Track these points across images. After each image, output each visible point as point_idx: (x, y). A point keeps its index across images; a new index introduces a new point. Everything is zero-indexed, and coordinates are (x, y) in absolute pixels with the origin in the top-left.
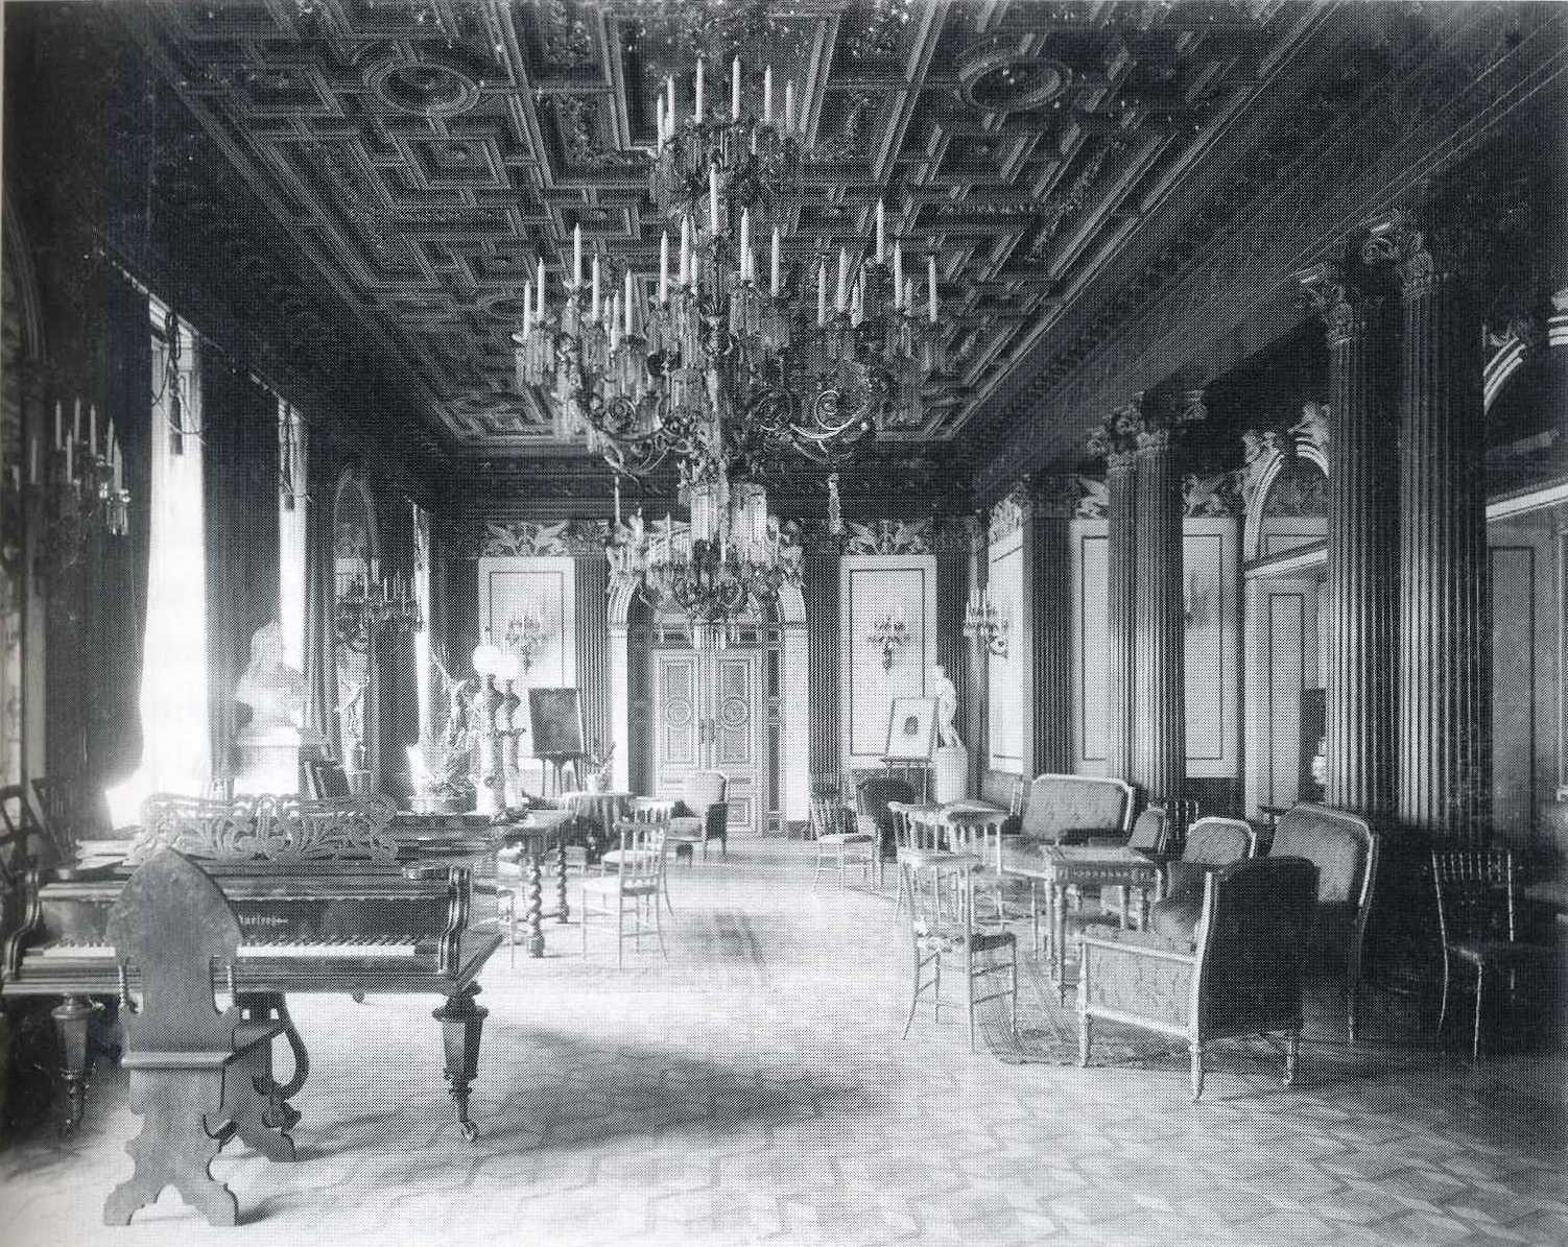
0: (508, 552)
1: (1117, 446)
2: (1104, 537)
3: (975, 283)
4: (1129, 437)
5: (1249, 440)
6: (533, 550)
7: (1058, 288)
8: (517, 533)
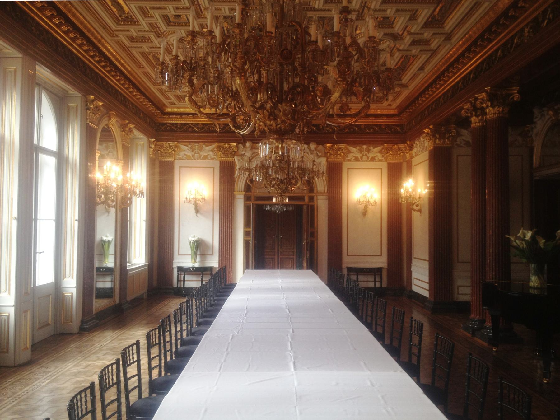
0: (357, 159)
1: (476, 113)
2: (469, 155)
3: (410, 33)
4: (483, 109)
5: (536, 111)
6: (368, 158)
7: (448, 37)
8: (361, 151)
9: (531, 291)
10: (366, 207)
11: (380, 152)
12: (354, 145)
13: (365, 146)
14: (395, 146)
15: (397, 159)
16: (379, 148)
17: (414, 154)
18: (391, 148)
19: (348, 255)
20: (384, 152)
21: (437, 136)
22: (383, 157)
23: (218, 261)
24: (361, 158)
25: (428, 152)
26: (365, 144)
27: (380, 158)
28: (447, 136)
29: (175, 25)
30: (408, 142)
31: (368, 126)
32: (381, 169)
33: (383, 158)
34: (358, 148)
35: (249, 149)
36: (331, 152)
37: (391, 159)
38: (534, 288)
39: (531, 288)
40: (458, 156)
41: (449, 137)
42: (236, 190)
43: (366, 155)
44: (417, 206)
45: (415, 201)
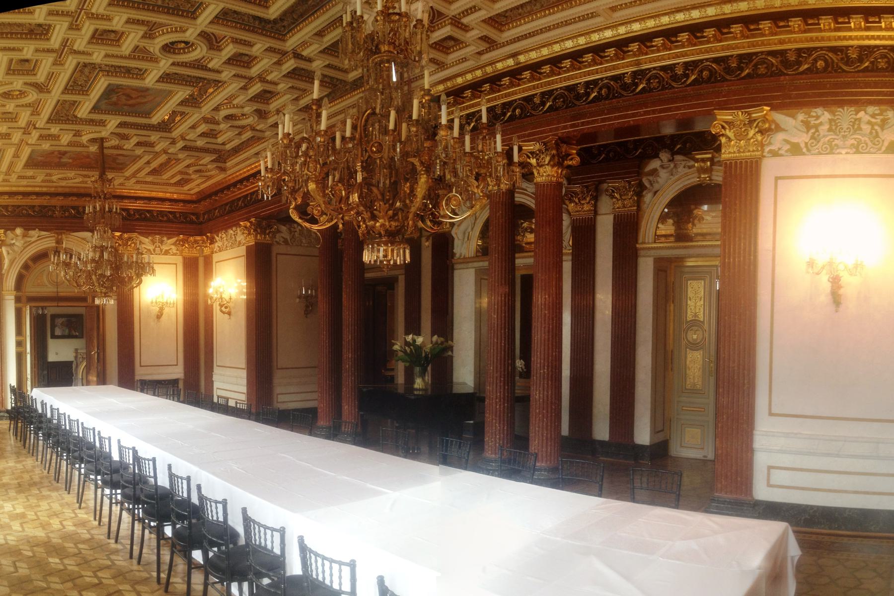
6: (161, 250)
8: (153, 242)
11: (174, 244)
14: (192, 239)
16: (174, 240)
17: (216, 249)
23: (473, 370)
24: (154, 250)
25: (244, 247)
26: (156, 234)
29: (14, 74)
31: (161, 213)
35: (20, 238)
37: (187, 252)
38: (419, 390)
39: (417, 390)
42: (4, 289)
44: (226, 308)
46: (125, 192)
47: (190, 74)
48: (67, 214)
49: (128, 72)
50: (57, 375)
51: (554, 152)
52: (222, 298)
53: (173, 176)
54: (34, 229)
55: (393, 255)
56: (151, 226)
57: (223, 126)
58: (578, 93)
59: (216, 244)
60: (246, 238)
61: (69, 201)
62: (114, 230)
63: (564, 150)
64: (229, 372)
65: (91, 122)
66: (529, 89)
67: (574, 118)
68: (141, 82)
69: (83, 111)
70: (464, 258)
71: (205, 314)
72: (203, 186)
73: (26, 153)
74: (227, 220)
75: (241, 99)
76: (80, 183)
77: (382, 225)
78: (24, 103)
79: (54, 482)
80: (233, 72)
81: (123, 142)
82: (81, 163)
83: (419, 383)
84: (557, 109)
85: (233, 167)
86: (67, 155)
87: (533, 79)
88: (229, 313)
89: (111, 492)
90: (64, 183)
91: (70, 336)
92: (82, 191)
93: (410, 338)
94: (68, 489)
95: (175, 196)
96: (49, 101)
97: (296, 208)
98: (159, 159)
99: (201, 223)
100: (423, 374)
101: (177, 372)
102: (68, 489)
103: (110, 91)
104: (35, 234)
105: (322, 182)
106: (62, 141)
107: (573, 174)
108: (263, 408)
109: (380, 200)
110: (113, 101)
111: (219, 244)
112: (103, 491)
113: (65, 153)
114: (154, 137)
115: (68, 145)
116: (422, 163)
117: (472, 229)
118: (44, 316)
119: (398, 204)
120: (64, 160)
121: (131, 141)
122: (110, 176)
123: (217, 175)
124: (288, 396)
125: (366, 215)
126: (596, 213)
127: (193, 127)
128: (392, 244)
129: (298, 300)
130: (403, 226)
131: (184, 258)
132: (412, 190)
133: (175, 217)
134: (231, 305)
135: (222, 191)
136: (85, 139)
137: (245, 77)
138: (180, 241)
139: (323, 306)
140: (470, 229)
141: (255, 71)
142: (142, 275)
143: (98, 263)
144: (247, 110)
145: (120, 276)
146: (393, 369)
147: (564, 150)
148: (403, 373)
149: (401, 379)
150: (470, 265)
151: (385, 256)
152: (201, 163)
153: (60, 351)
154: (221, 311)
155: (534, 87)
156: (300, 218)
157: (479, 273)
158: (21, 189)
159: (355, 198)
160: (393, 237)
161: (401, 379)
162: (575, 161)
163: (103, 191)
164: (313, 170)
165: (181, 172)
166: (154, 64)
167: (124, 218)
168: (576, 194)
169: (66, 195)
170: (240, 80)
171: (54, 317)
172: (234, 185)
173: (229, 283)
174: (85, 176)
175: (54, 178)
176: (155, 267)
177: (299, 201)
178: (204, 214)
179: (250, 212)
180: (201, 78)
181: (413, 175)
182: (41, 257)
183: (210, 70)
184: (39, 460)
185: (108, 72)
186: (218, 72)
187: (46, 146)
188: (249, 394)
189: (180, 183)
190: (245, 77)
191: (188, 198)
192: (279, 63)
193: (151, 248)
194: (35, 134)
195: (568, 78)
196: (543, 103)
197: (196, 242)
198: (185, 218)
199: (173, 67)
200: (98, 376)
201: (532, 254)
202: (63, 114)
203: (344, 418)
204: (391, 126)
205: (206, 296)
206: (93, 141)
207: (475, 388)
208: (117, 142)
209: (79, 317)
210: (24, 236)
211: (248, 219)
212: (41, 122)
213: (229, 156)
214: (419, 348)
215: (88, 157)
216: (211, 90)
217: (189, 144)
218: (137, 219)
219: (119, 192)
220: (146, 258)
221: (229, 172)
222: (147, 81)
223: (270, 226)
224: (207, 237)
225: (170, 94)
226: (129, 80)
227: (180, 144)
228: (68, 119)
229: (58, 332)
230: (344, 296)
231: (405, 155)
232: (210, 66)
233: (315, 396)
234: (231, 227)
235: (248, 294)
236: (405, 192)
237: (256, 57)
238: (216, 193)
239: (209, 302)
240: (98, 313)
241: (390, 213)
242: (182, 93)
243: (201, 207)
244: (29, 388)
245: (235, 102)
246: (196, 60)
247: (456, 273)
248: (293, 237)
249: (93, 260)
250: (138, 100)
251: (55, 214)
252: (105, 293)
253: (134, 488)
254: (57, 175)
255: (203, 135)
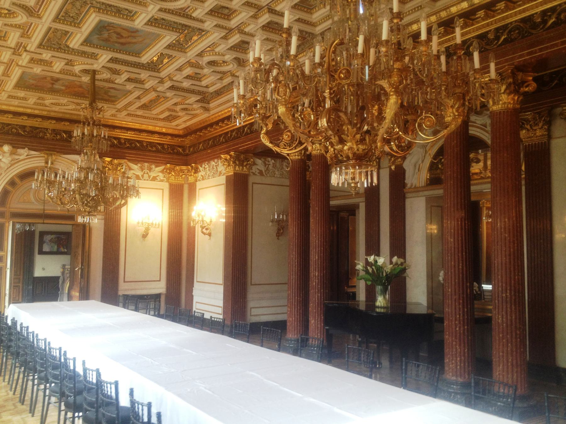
0: (138, 177)
6: (149, 177)
9: (378, 310)
10: (147, 229)
11: (162, 172)
12: (135, 162)
13: (146, 164)
14: (178, 168)
15: (180, 180)
18: (174, 169)
19: (124, 282)
20: (166, 172)
21: (237, 163)
22: (164, 177)
24: (143, 176)
25: (224, 177)
26: (146, 162)
27: (162, 178)
28: (245, 164)
30: (193, 165)
31: (151, 144)
32: (163, 189)
33: (165, 179)
34: (139, 165)
35: (8, 155)
36: (110, 167)
37: (173, 180)
38: (381, 307)
39: (378, 307)
40: (253, 183)
41: (247, 164)
43: (147, 173)
44: (207, 229)
45: (206, 225)
46: (117, 123)
47: (176, 21)
48: (58, 137)
49: (118, 11)
50: (43, 290)
51: (511, 80)
52: (203, 221)
53: (162, 112)
54: (24, 148)
55: (360, 178)
56: (140, 155)
57: (206, 71)
58: (535, 23)
59: (200, 174)
60: (226, 169)
61: (65, 126)
62: (102, 155)
63: (519, 78)
64: (207, 287)
65: (83, 54)
66: (483, 27)
67: (532, 46)
68: (131, 22)
69: (75, 42)
70: (415, 187)
71: (188, 235)
72: (188, 124)
73: (16, 74)
74: (209, 153)
75: (221, 48)
76: (74, 110)
77: (350, 148)
78: (10, 23)
79: (19, 405)
80: (215, 23)
81: (115, 76)
82: (74, 91)
83: (380, 301)
84: (512, 41)
85: (216, 107)
86: (60, 82)
87: (487, 17)
88: (210, 235)
89: (74, 415)
90: (56, 108)
91: (58, 253)
92: (75, 118)
93: (371, 259)
94: (32, 411)
95: (164, 130)
96: (40, 26)
97: (267, 133)
98: (149, 96)
99: (187, 155)
100: (384, 292)
101: (160, 287)
102: (32, 411)
103: (101, 28)
104: (24, 152)
105: (293, 108)
106: (54, 68)
107: (528, 101)
108: (238, 323)
109: (348, 124)
110: (104, 36)
111: (201, 173)
112: (66, 414)
113: (57, 80)
114: (144, 75)
115: (60, 72)
116: (391, 85)
117: (423, 161)
118: (31, 234)
119: (366, 128)
120: (57, 86)
121: (123, 76)
122: (100, 105)
123: (202, 114)
124: (261, 310)
125: (334, 140)
126: (550, 137)
127: (180, 69)
128: (360, 167)
129: (271, 224)
130: (370, 150)
131: (171, 185)
132: (380, 112)
133: (163, 148)
134: (211, 227)
135: (205, 128)
136: (77, 69)
137: (225, 28)
138: (167, 169)
139: (292, 230)
140: (420, 162)
141: (234, 23)
142: (127, 196)
143: (82, 183)
144: (228, 57)
145: (106, 198)
146: (355, 287)
147: (519, 78)
148: (364, 291)
149: (362, 296)
150: (421, 193)
151: (353, 179)
152: (187, 102)
153: (46, 266)
154: (203, 232)
155: (488, 25)
156: (271, 142)
157: (429, 200)
158: (12, 109)
159: (323, 123)
160: (361, 159)
161: (362, 296)
162: (532, 87)
163: (92, 118)
164: (284, 94)
165: (169, 109)
166: (144, 8)
167: (112, 145)
168: (528, 121)
169: (59, 120)
170: (222, 30)
171: (42, 234)
172: (217, 123)
173: (210, 206)
174: (78, 104)
175: (47, 102)
176: (140, 190)
177: (270, 126)
178: (190, 147)
179: (229, 147)
180: (186, 26)
181: (379, 97)
182: (27, 175)
183: (194, 19)
184: (7, 380)
185: (99, 9)
186: (202, 21)
187: (37, 70)
188: (225, 307)
189: (169, 119)
190: (225, 28)
191: (176, 132)
192: (255, 17)
193: (140, 173)
194: (25, 58)
195: (524, 11)
196: (497, 38)
197: (182, 170)
198: (173, 150)
199: (159, 13)
200: (81, 291)
201: (490, 180)
202: (54, 42)
203: (311, 333)
204: (360, 49)
205: (189, 217)
206: (86, 71)
207: (428, 307)
208: (109, 76)
209: (68, 235)
210: (12, 153)
211: (228, 153)
212: (33, 44)
213: (212, 98)
214: (380, 269)
215: (80, 87)
216: (195, 38)
217: (176, 84)
218: (128, 148)
219: (110, 122)
220: (131, 182)
221: (212, 112)
222: (137, 22)
223: (247, 159)
224: (192, 167)
225: (157, 38)
226: (120, 20)
227: (168, 84)
228: (60, 48)
229: (46, 248)
230: (311, 220)
231: (374, 77)
232: (194, 15)
233: (285, 309)
234: (213, 159)
235: (227, 217)
236: (373, 114)
237: (235, 11)
238: (200, 130)
239: (192, 224)
240: (85, 229)
241: (358, 136)
242: (169, 38)
243: (187, 141)
244: (7, 304)
245: (217, 50)
246: (181, 9)
247: (408, 202)
248: (267, 169)
249: (78, 180)
250: (129, 40)
251: (47, 136)
252: (89, 212)
253: (97, 411)
254: (49, 100)
255: (188, 77)
